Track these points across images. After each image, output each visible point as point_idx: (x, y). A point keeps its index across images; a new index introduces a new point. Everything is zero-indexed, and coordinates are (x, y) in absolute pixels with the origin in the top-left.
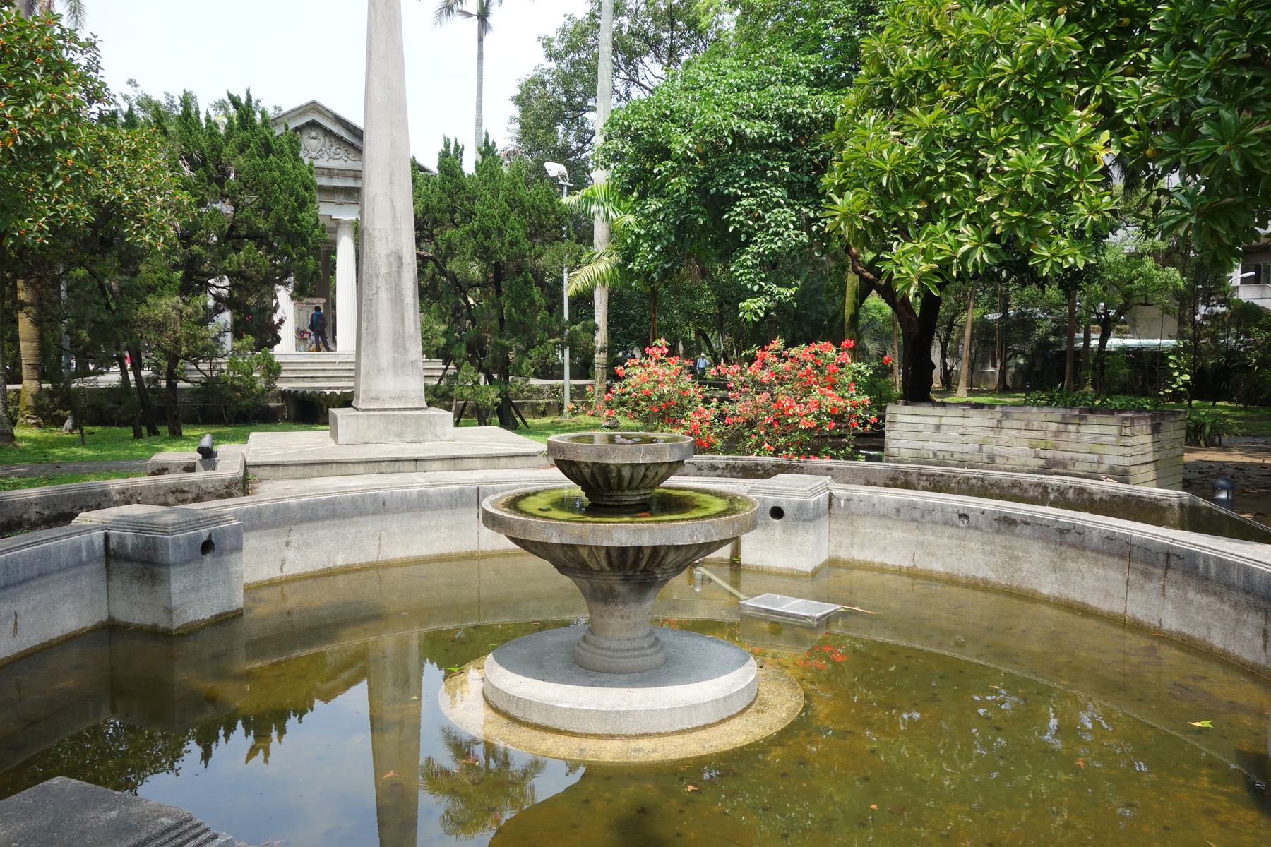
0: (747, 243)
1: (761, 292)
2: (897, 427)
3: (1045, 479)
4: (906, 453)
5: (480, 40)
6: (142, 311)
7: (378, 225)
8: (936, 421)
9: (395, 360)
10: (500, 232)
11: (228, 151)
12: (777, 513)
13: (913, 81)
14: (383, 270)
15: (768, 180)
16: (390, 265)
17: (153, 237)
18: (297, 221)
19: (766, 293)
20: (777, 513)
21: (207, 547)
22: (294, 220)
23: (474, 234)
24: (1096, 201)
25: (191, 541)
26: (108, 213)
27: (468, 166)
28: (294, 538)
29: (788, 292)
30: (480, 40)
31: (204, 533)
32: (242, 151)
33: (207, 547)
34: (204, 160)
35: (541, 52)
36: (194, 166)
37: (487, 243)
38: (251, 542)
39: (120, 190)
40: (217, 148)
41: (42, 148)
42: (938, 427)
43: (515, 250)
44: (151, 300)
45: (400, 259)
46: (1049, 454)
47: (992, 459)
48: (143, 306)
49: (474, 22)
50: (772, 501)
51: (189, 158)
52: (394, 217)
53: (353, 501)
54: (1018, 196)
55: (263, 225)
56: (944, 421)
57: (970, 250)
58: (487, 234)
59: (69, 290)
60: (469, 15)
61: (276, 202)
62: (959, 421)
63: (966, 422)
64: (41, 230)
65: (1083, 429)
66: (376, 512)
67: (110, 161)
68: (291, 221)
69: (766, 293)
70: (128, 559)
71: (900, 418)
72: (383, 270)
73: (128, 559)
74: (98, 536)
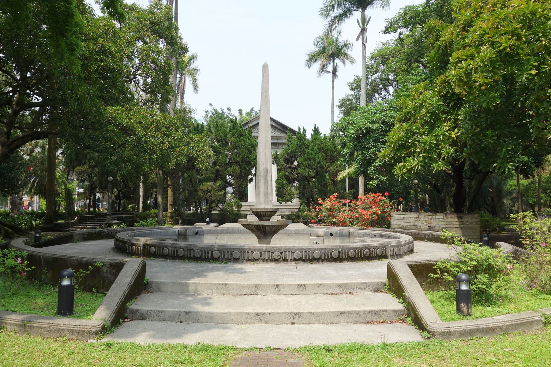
0: (373, 163)
1: (377, 178)
2: (394, 218)
3: (426, 232)
4: (396, 226)
5: (333, 81)
6: (201, 187)
7: (261, 160)
8: (403, 216)
9: (265, 200)
10: (314, 159)
11: (229, 136)
12: (331, 235)
13: (408, 114)
14: (262, 174)
15: (380, 142)
16: (264, 172)
17: (202, 166)
18: (248, 157)
19: (378, 179)
20: (331, 235)
21: (197, 233)
22: (248, 157)
23: (305, 160)
24: (449, 150)
25: (194, 231)
26: (191, 160)
27: (309, 136)
28: (218, 237)
29: (384, 178)
30: (333, 81)
31: (196, 230)
32: (233, 136)
33: (197, 233)
34: (221, 140)
35: (348, 88)
36: (218, 142)
37: (310, 162)
38: (206, 236)
39: (194, 152)
40: (225, 136)
41: (173, 148)
42: (404, 218)
43: (319, 165)
44: (204, 183)
45: (267, 170)
46: (429, 225)
47: (417, 227)
48: (202, 186)
49: (331, 75)
50: (330, 232)
51: (217, 139)
52: (266, 158)
53: (233, 229)
54: (425, 151)
55: (238, 159)
56: (406, 216)
57: (416, 165)
58: (310, 160)
59: (182, 181)
60: (329, 72)
61: (242, 151)
62: (409, 216)
63: (411, 216)
64: (173, 165)
65: (437, 217)
66: (238, 233)
67: (192, 144)
68: (247, 158)
69: (378, 179)
70: (182, 235)
71: (394, 215)
72: (262, 174)
73: (182, 235)
74: (177, 230)
